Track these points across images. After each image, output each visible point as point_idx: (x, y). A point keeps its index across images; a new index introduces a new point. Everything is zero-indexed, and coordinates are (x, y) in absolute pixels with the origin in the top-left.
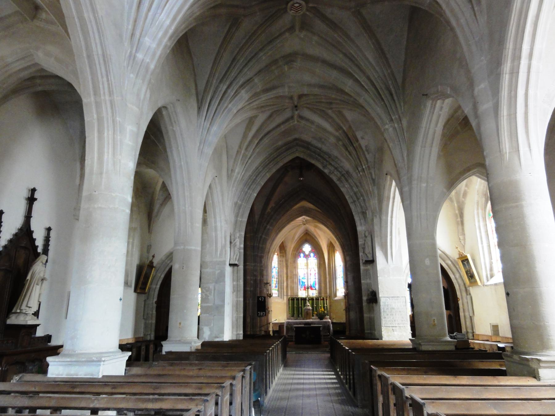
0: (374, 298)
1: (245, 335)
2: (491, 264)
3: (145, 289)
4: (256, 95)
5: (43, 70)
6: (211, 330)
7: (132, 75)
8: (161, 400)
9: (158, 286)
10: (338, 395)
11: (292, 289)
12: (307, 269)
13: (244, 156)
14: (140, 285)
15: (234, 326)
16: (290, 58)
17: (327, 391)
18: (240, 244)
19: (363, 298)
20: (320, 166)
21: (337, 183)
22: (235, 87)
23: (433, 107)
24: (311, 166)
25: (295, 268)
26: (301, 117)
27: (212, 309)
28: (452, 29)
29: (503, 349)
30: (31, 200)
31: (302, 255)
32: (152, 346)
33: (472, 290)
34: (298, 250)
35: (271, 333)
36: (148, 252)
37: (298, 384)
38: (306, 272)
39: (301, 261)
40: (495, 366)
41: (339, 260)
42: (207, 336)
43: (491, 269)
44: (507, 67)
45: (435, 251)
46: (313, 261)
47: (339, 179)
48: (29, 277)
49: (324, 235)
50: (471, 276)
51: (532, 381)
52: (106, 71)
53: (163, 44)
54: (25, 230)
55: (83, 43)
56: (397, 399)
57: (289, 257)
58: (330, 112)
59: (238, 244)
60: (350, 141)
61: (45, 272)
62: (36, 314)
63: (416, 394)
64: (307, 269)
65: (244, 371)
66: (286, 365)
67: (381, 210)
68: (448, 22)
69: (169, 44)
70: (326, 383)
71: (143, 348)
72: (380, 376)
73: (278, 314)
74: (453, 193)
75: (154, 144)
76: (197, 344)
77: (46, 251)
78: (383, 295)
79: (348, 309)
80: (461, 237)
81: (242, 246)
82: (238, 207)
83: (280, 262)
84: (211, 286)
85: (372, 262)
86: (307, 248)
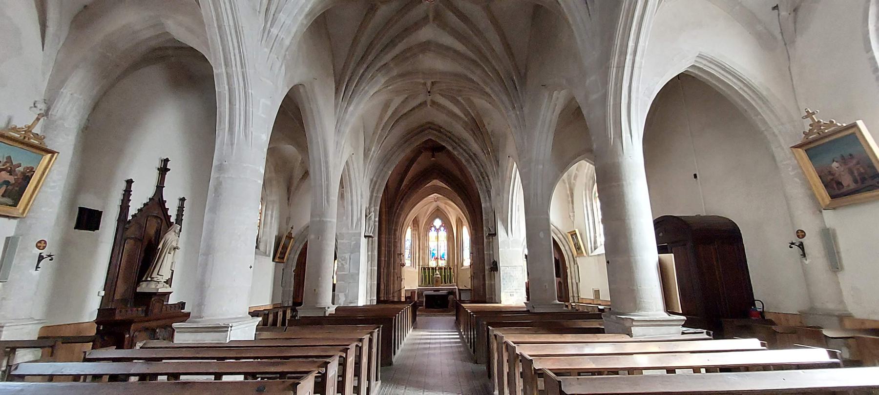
0: (495, 267)
1: (379, 301)
2: (595, 237)
3: (283, 258)
4: (393, 79)
5: (174, 40)
6: (346, 296)
7: (266, 50)
8: (282, 364)
9: (297, 256)
10: (460, 352)
11: (424, 259)
12: (437, 242)
13: (381, 136)
14: (278, 255)
15: (368, 292)
16: (425, 47)
17: (444, 351)
18: (375, 217)
19: (486, 266)
20: (450, 148)
21: (465, 164)
22: (372, 71)
23: (551, 96)
24: (442, 149)
25: (428, 240)
26: (433, 103)
27: (349, 278)
28: (569, 26)
29: (602, 310)
30: (163, 170)
31: (433, 229)
32: (289, 312)
33: (578, 260)
34: (429, 225)
35: (403, 299)
36: (287, 223)
37: (425, 343)
38: (434, 243)
39: (432, 234)
40: (595, 324)
41: (466, 234)
42: (342, 301)
43: (595, 242)
44: (615, 61)
45: (549, 226)
46: (443, 234)
47: (467, 161)
48: (160, 246)
49: (454, 211)
50: (578, 248)
51: (627, 338)
52: (238, 42)
53: (299, 22)
54: (157, 199)
55: (213, 13)
56: (509, 356)
57: (422, 229)
58: (459, 98)
59: (373, 217)
60: (477, 127)
61: (177, 241)
62: (169, 282)
63: (526, 351)
64: (437, 242)
65: (371, 334)
66: (415, 328)
67: (504, 190)
68: (566, 20)
69: (305, 22)
70: (450, 343)
71: (280, 314)
72: (495, 336)
73: (411, 280)
74: (565, 175)
75: (292, 119)
76: (332, 310)
77: (179, 220)
78: (502, 265)
79: (473, 277)
80: (571, 214)
81: (377, 219)
82: (373, 184)
83: (413, 236)
84: (347, 256)
85: (494, 234)
86: (438, 223)
